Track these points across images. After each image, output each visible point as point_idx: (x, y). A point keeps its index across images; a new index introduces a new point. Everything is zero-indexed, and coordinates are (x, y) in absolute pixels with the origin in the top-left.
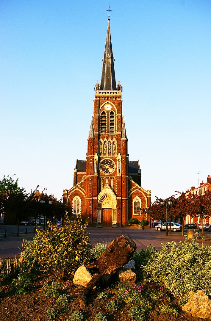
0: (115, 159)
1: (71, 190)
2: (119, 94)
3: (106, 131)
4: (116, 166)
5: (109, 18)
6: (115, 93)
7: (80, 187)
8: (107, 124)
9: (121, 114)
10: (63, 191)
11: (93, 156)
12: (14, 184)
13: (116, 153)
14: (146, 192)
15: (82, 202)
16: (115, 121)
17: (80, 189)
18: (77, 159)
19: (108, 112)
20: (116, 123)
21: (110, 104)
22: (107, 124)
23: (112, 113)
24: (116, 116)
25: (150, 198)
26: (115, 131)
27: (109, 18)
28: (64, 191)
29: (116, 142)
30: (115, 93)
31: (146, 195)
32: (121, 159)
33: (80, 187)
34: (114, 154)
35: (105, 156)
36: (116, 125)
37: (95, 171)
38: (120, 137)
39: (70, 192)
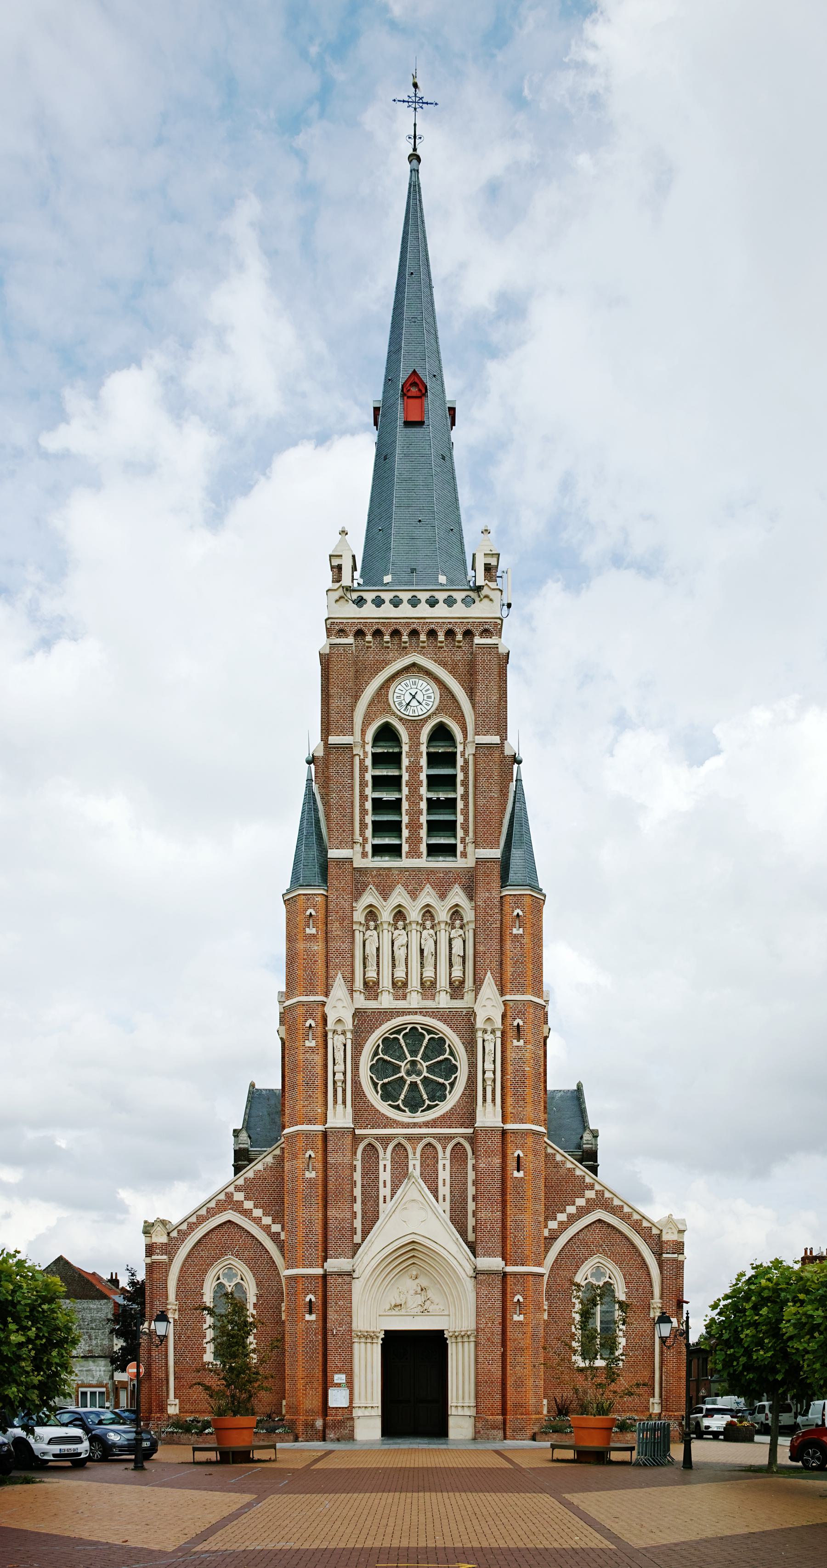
0: (466, 1023)
1: (203, 1212)
2: (481, 611)
3: (405, 848)
4: (472, 1065)
5: (415, 149)
6: (459, 605)
7: (249, 1205)
8: (414, 787)
9: (501, 729)
10: (141, 1226)
11: (323, 1004)
12: (261, 1210)
13: (469, 983)
14: (655, 1231)
15: (258, 1297)
16: (465, 784)
17: (247, 1213)
18: (252, 1085)
19: (415, 725)
20: (465, 797)
21: (428, 673)
22: (414, 787)
23: (441, 733)
24: (470, 750)
25: (679, 1267)
26: (460, 848)
27: (415, 149)
28: (148, 1229)
29: (469, 915)
30: (459, 605)
31: (658, 1246)
32: (504, 1016)
33: (249, 1205)
34: (456, 989)
35: (401, 1004)
36: (466, 805)
37: (340, 1090)
38: (496, 883)
39: (183, 1235)
